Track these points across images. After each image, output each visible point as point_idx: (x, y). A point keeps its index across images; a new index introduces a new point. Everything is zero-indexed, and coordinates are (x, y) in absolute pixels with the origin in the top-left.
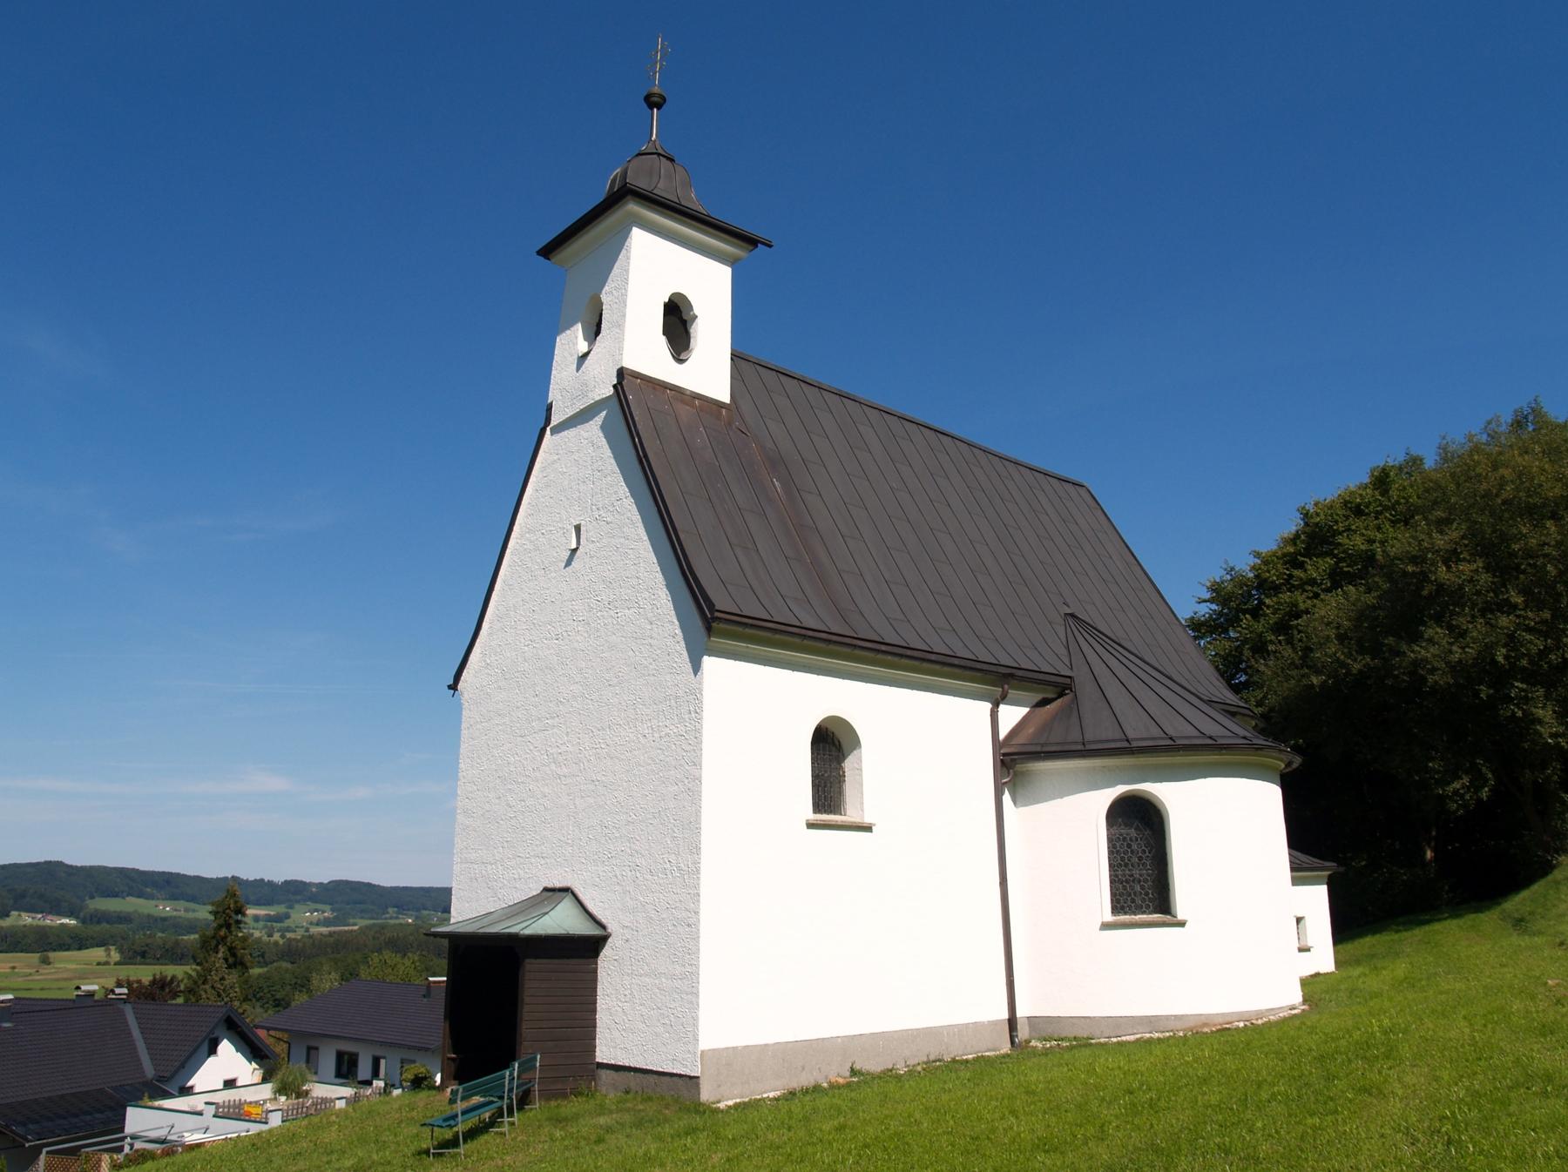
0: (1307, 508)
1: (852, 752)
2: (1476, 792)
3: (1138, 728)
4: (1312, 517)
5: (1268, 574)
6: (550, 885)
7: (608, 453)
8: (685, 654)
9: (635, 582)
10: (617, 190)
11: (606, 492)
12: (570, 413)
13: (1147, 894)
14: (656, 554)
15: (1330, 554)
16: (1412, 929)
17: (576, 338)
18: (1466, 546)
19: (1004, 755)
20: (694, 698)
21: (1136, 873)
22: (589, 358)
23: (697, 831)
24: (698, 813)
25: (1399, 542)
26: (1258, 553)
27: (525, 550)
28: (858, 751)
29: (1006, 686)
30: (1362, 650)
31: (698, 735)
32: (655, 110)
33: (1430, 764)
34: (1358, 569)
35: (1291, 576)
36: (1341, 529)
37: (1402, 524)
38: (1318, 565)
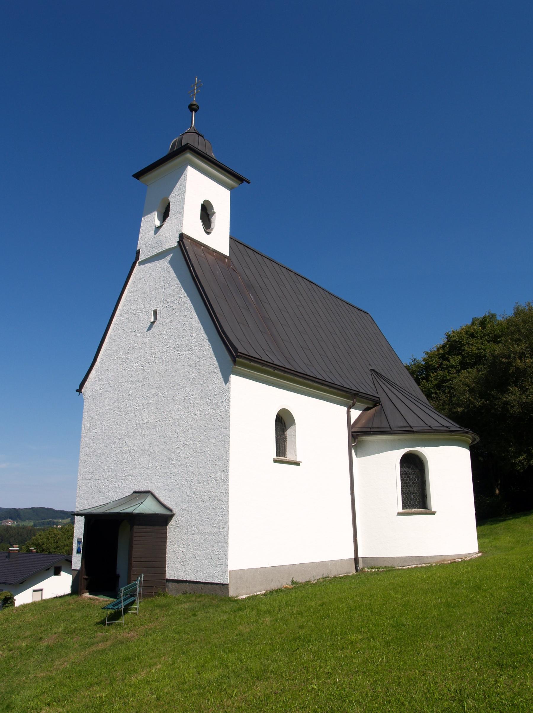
0: (449, 333)
1: (290, 427)
2: (528, 462)
3: (414, 422)
4: (451, 338)
5: (432, 362)
6: (138, 490)
7: (174, 274)
8: (220, 374)
9: (190, 338)
10: (176, 150)
11: (172, 294)
12: (150, 255)
13: (416, 500)
14: (202, 325)
15: (460, 354)
16: (499, 523)
17: (154, 218)
18: (528, 351)
19: (353, 432)
20: (226, 395)
21: (411, 489)
22: (162, 228)
23: (227, 461)
24: (228, 453)
25: (498, 349)
26: (427, 353)
27: (123, 322)
28: (294, 426)
29: (355, 400)
30: (481, 397)
31: (227, 414)
32: (194, 112)
33: (510, 449)
34: (473, 361)
35: (442, 364)
36: (465, 343)
37: (493, 342)
38: (455, 359)
